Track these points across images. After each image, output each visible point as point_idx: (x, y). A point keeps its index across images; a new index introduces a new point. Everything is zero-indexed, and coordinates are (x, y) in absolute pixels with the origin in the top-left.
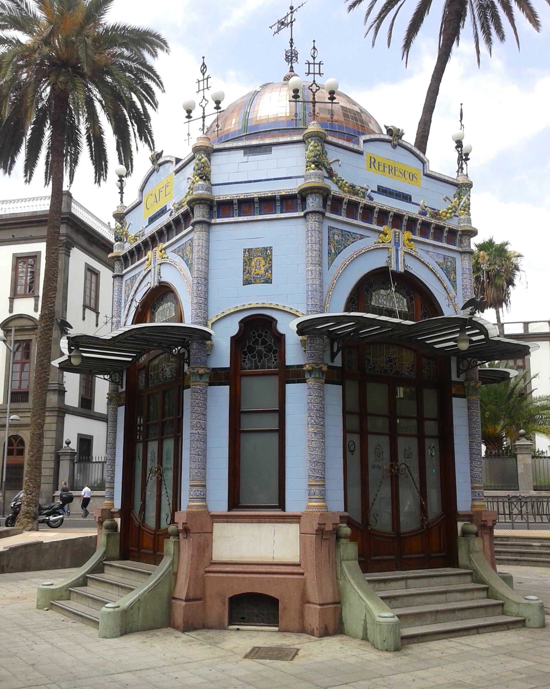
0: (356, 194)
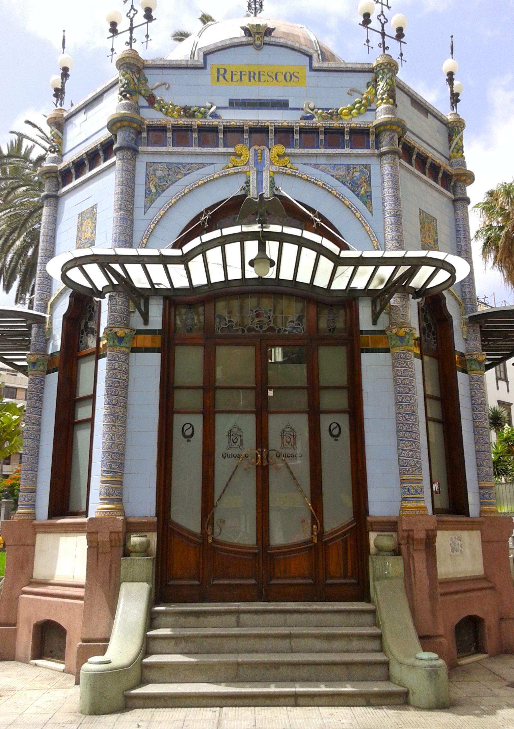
0: (193, 115)
